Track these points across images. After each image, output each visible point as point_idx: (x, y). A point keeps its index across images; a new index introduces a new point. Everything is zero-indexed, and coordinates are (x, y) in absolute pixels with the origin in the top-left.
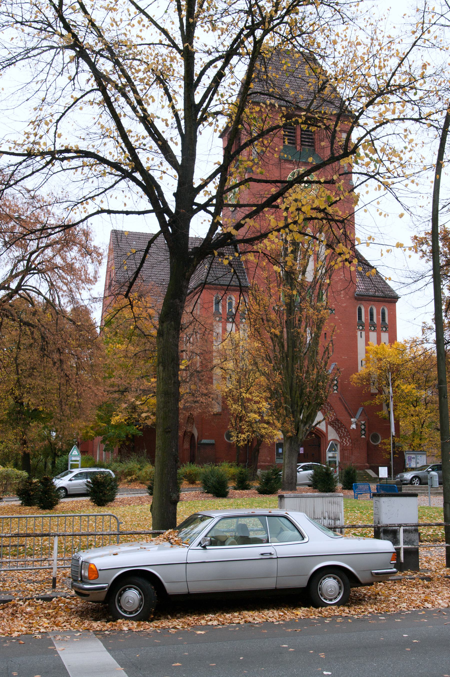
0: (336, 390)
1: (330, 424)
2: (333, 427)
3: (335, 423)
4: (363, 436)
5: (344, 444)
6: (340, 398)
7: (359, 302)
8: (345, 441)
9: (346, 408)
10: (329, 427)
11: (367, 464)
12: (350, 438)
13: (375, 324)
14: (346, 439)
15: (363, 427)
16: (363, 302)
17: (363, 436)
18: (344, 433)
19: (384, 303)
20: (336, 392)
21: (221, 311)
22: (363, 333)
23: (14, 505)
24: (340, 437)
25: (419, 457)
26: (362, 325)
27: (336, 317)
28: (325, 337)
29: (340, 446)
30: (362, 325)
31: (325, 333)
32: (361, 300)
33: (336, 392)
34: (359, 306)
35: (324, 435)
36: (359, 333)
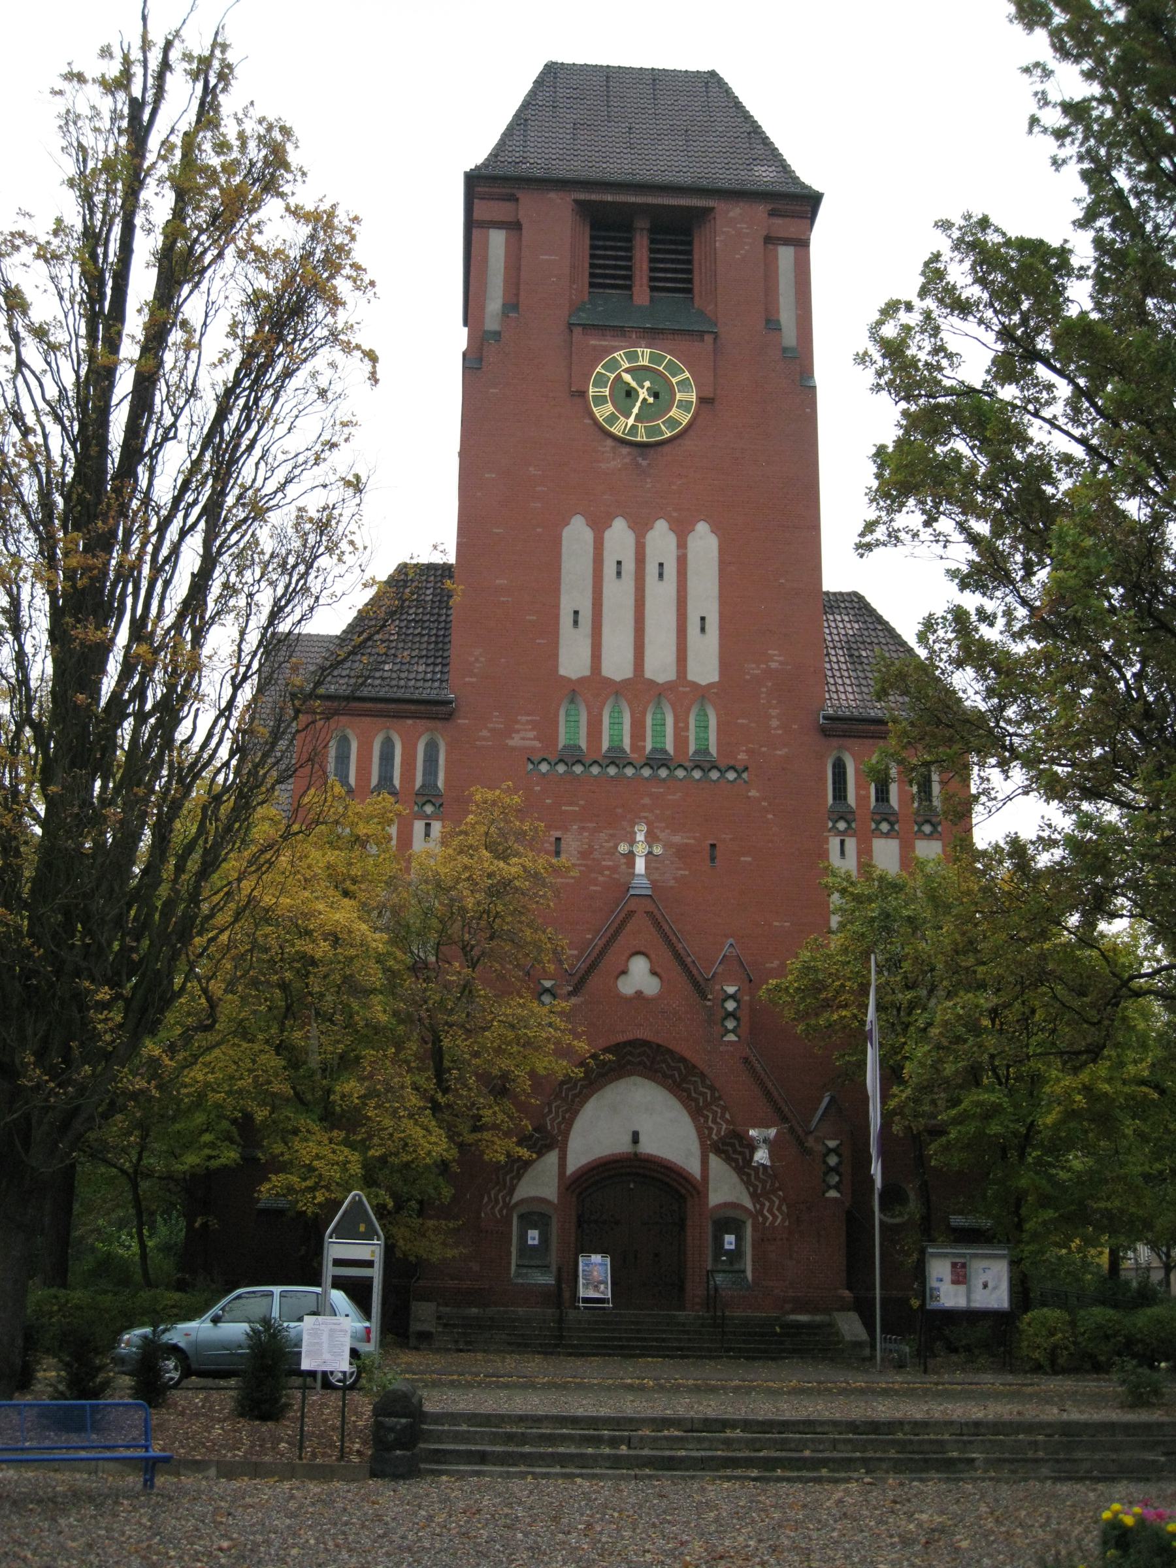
0: (733, 1031)
1: (718, 1152)
2: (728, 1160)
3: (733, 1145)
4: (833, 1194)
5: (766, 1219)
6: (746, 1060)
7: (835, 742)
8: (770, 1211)
9: (768, 1094)
10: (715, 1161)
11: (846, 1293)
12: (783, 1200)
13: (894, 814)
14: (772, 1202)
15: (833, 1160)
16: (849, 742)
17: (833, 1194)
18: (764, 1182)
19: (388, 722)
20: (732, 1037)
21: (397, 782)
22: (851, 844)
23: (808, 1470)
24: (754, 1196)
25: (977, 1266)
26: (846, 815)
27: (753, 793)
28: (713, 859)
29: (753, 1226)
30: (846, 815)
31: (713, 846)
32: (846, 735)
33: (732, 1037)
34: (835, 754)
35: (694, 1187)
36: (834, 843)
